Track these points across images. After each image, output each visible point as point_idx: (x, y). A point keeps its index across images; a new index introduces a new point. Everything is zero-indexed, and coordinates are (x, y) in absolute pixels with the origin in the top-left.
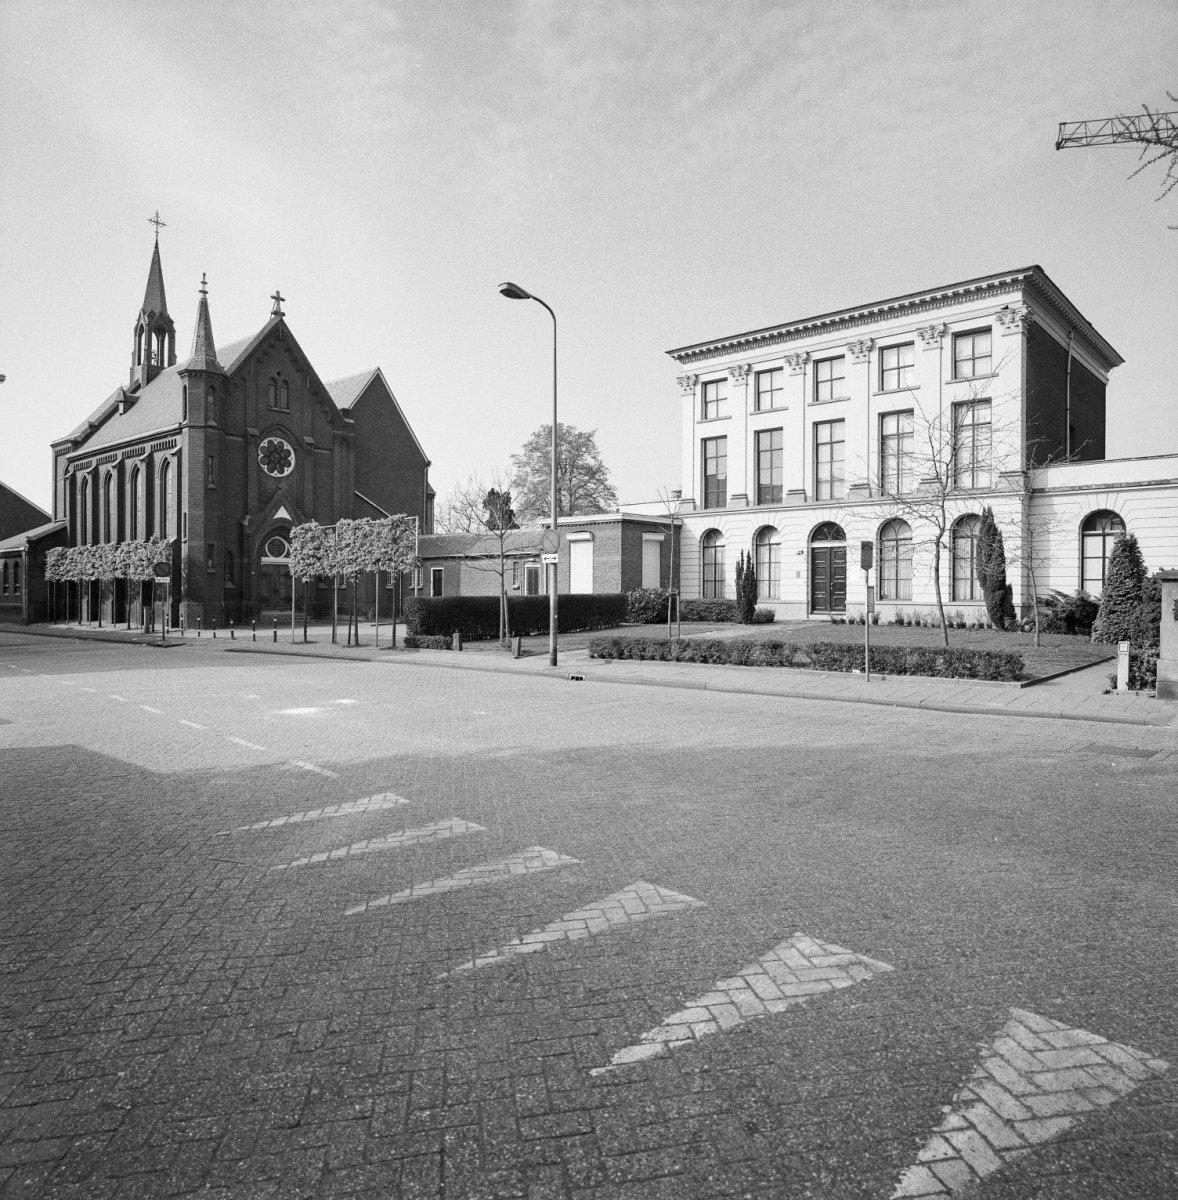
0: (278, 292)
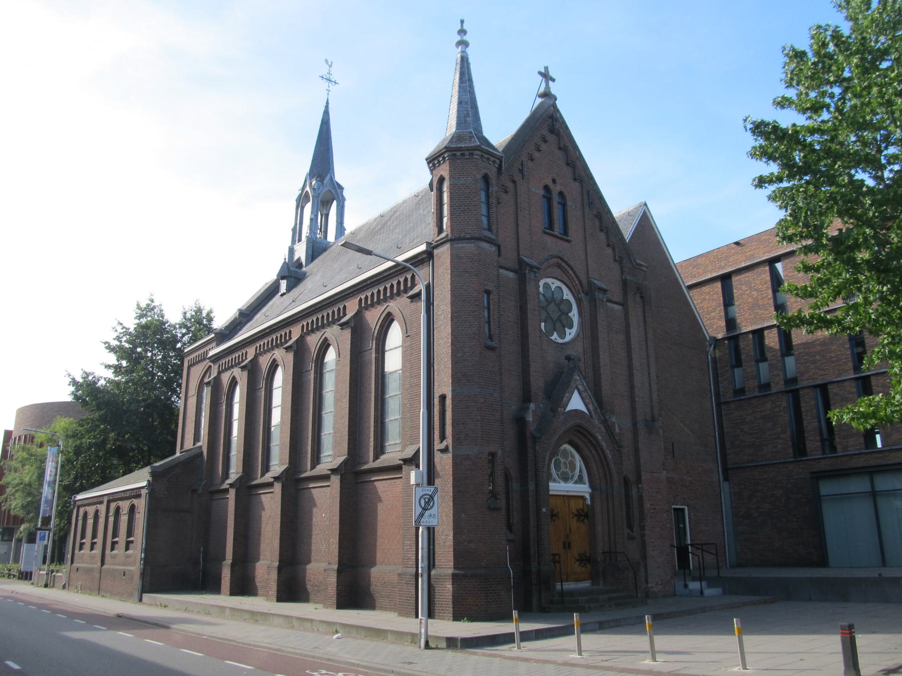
0: (546, 68)
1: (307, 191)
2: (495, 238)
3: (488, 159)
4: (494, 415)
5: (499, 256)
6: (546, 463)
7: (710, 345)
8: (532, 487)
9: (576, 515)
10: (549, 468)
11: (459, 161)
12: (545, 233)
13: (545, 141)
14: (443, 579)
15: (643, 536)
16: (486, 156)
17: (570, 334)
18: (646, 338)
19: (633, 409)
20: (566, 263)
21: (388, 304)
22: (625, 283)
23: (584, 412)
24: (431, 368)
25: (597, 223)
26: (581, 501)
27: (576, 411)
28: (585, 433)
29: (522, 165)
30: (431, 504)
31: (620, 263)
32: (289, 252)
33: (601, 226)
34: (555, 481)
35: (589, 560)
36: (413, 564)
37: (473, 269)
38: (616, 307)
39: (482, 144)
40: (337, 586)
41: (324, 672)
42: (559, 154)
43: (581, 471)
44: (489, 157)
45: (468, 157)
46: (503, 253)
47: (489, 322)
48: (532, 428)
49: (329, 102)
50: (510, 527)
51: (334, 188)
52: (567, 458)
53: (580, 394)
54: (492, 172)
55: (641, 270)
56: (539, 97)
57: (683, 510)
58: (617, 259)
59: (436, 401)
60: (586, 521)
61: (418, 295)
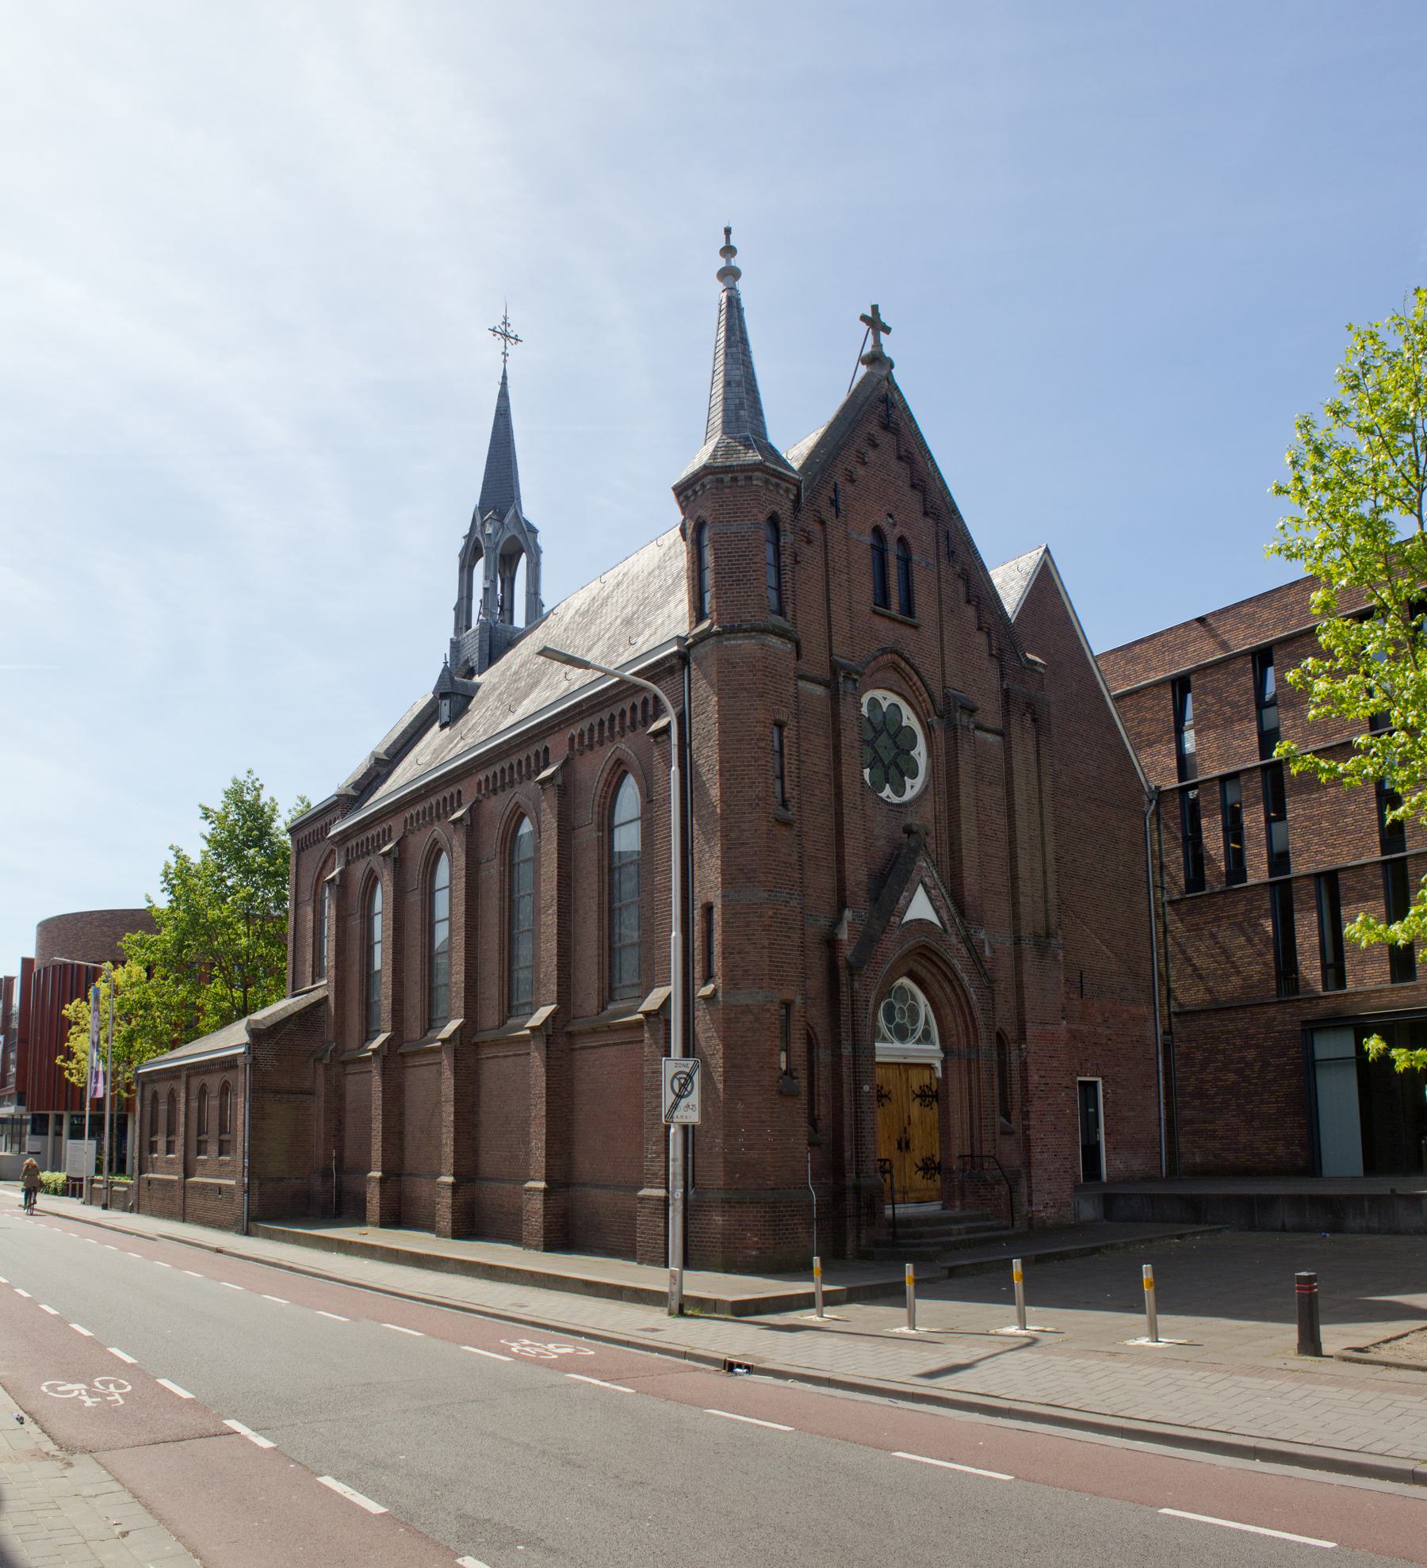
0: (875, 308)
1: (477, 538)
2: (791, 629)
3: (777, 485)
4: (789, 937)
5: (798, 660)
6: (871, 1007)
7: (1151, 801)
8: (847, 1050)
9: (918, 1096)
10: (875, 1019)
11: (727, 491)
12: (875, 612)
13: (875, 446)
14: (707, 1206)
15: (1026, 1128)
16: (774, 480)
17: (912, 787)
18: (1040, 791)
19: (1016, 916)
20: (907, 661)
21: (618, 745)
22: (1006, 694)
23: (932, 923)
24: (687, 857)
25: (962, 589)
26: (927, 1073)
27: (920, 921)
28: (934, 958)
29: (835, 491)
30: (689, 1089)
31: (1000, 659)
32: (451, 648)
33: (968, 594)
34: (884, 1039)
35: (938, 1168)
36: (660, 1183)
37: (755, 684)
38: (990, 738)
39: (766, 459)
40: (545, 1216)
41: (527, 1342)
42: (897, 467)
43: (927, 1022)
44: (778, 481)
45: (743, 483)
46: (804, 652)
47: (781, 777)
48: (847, 951)
49: (508, 375)
50: (813, 1122)
51: (522, 532)
52: (905, 1002)
53: (928, 892)
54: (785, 511)
55: (1036, 671)
56: (863, 363)
57: (1095, 1083)
58: (994, 652)
59: (697, 914)
60: (935, 1105)
61: (666, 730)
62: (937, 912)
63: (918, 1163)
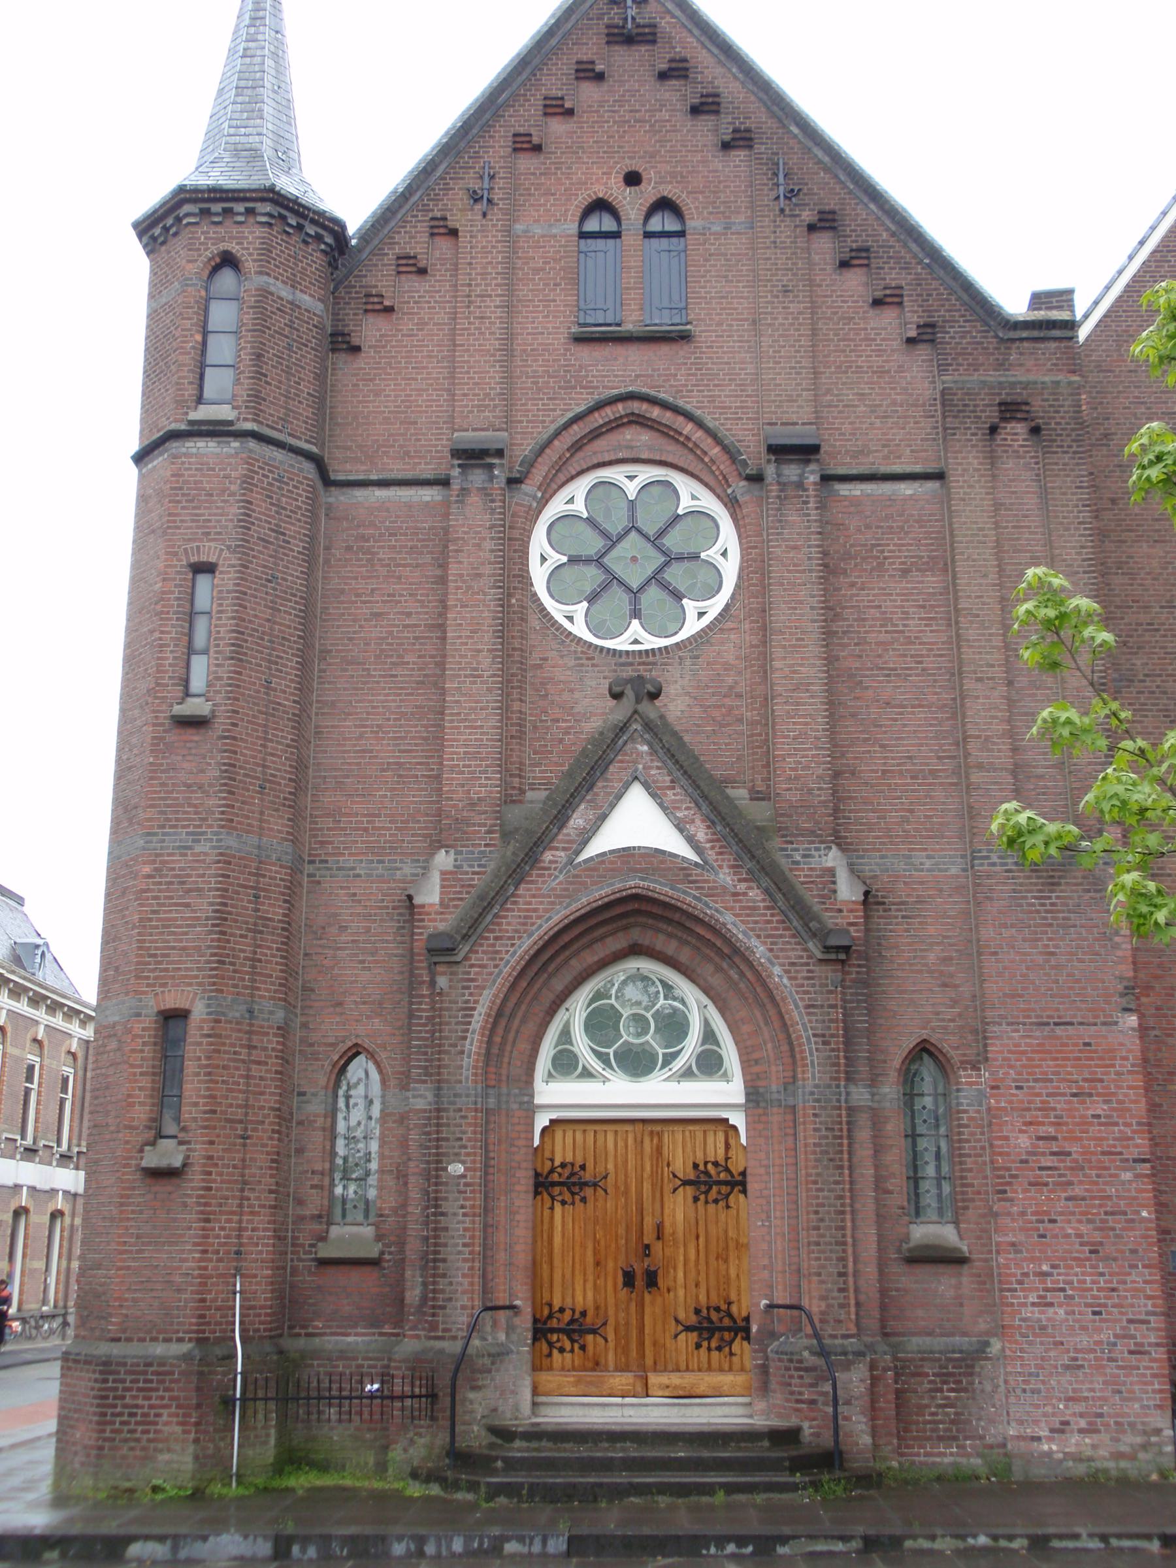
4: (187, 905)
9: (686, 1183)
62: (680, 827)
63: (682, 1316)
